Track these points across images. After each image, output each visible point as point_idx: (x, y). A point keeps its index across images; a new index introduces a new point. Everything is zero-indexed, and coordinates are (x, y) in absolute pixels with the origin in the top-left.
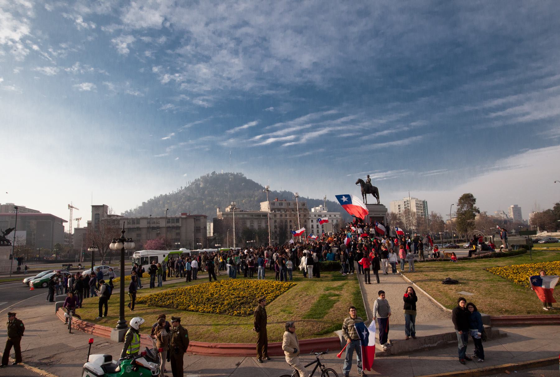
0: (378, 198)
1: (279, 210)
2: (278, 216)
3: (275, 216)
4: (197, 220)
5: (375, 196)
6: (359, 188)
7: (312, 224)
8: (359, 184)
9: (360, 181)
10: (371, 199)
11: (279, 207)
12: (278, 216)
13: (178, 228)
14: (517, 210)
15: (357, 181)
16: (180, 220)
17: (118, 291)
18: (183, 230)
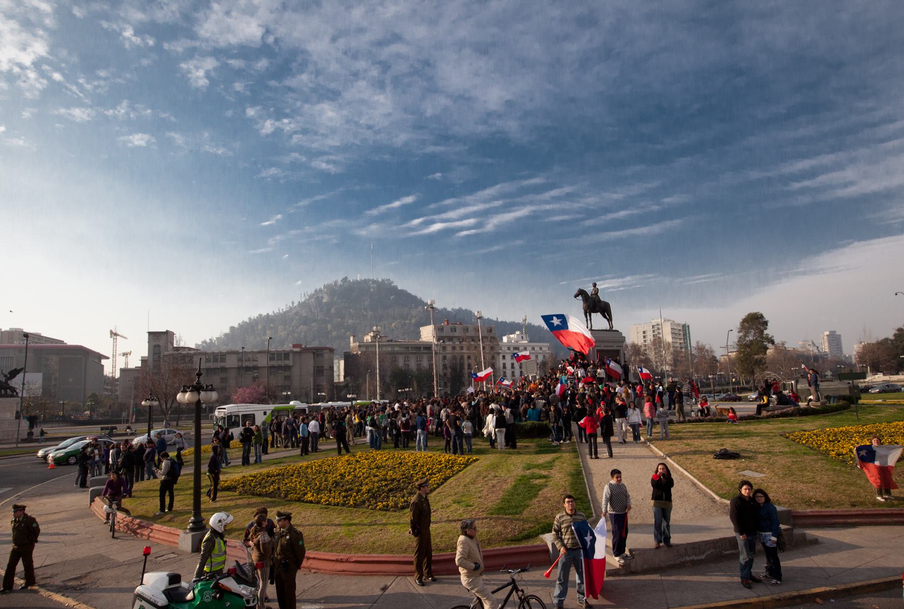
0: (610, 320)
1: (450, 339)
2: (449, 349)
3: (444, 348)
4: (318, 355)
5: (605, 317)
6: (580, 303)
7: (504, 361)
8: (580, 297)
9: (581, 293)
10: (599, 321)
11: (451, 334)
12: (449, 349)
13: (288, 368)
14: (834, 339)
15: (576, 292)
16: (291, 355)
17: (191, 470)
18: (295, 371)
